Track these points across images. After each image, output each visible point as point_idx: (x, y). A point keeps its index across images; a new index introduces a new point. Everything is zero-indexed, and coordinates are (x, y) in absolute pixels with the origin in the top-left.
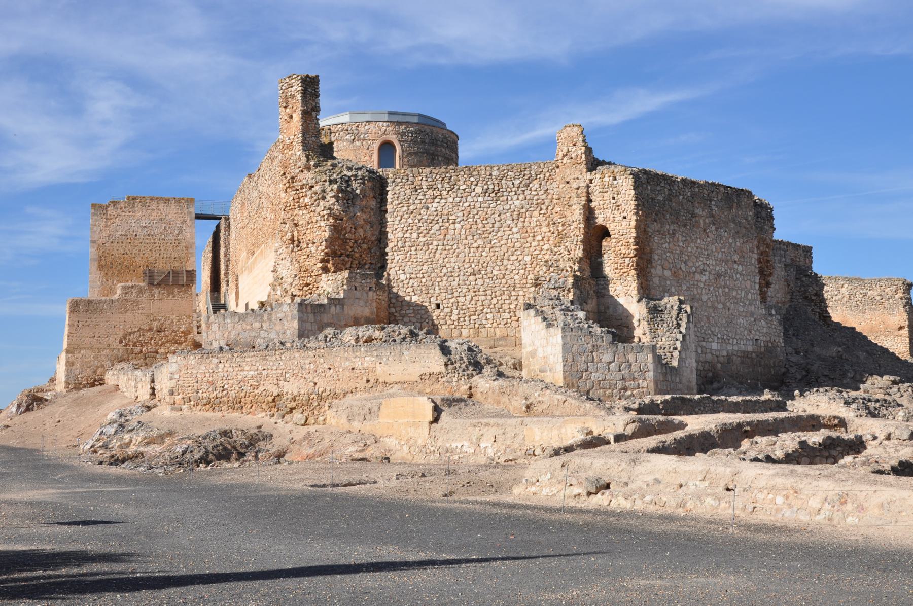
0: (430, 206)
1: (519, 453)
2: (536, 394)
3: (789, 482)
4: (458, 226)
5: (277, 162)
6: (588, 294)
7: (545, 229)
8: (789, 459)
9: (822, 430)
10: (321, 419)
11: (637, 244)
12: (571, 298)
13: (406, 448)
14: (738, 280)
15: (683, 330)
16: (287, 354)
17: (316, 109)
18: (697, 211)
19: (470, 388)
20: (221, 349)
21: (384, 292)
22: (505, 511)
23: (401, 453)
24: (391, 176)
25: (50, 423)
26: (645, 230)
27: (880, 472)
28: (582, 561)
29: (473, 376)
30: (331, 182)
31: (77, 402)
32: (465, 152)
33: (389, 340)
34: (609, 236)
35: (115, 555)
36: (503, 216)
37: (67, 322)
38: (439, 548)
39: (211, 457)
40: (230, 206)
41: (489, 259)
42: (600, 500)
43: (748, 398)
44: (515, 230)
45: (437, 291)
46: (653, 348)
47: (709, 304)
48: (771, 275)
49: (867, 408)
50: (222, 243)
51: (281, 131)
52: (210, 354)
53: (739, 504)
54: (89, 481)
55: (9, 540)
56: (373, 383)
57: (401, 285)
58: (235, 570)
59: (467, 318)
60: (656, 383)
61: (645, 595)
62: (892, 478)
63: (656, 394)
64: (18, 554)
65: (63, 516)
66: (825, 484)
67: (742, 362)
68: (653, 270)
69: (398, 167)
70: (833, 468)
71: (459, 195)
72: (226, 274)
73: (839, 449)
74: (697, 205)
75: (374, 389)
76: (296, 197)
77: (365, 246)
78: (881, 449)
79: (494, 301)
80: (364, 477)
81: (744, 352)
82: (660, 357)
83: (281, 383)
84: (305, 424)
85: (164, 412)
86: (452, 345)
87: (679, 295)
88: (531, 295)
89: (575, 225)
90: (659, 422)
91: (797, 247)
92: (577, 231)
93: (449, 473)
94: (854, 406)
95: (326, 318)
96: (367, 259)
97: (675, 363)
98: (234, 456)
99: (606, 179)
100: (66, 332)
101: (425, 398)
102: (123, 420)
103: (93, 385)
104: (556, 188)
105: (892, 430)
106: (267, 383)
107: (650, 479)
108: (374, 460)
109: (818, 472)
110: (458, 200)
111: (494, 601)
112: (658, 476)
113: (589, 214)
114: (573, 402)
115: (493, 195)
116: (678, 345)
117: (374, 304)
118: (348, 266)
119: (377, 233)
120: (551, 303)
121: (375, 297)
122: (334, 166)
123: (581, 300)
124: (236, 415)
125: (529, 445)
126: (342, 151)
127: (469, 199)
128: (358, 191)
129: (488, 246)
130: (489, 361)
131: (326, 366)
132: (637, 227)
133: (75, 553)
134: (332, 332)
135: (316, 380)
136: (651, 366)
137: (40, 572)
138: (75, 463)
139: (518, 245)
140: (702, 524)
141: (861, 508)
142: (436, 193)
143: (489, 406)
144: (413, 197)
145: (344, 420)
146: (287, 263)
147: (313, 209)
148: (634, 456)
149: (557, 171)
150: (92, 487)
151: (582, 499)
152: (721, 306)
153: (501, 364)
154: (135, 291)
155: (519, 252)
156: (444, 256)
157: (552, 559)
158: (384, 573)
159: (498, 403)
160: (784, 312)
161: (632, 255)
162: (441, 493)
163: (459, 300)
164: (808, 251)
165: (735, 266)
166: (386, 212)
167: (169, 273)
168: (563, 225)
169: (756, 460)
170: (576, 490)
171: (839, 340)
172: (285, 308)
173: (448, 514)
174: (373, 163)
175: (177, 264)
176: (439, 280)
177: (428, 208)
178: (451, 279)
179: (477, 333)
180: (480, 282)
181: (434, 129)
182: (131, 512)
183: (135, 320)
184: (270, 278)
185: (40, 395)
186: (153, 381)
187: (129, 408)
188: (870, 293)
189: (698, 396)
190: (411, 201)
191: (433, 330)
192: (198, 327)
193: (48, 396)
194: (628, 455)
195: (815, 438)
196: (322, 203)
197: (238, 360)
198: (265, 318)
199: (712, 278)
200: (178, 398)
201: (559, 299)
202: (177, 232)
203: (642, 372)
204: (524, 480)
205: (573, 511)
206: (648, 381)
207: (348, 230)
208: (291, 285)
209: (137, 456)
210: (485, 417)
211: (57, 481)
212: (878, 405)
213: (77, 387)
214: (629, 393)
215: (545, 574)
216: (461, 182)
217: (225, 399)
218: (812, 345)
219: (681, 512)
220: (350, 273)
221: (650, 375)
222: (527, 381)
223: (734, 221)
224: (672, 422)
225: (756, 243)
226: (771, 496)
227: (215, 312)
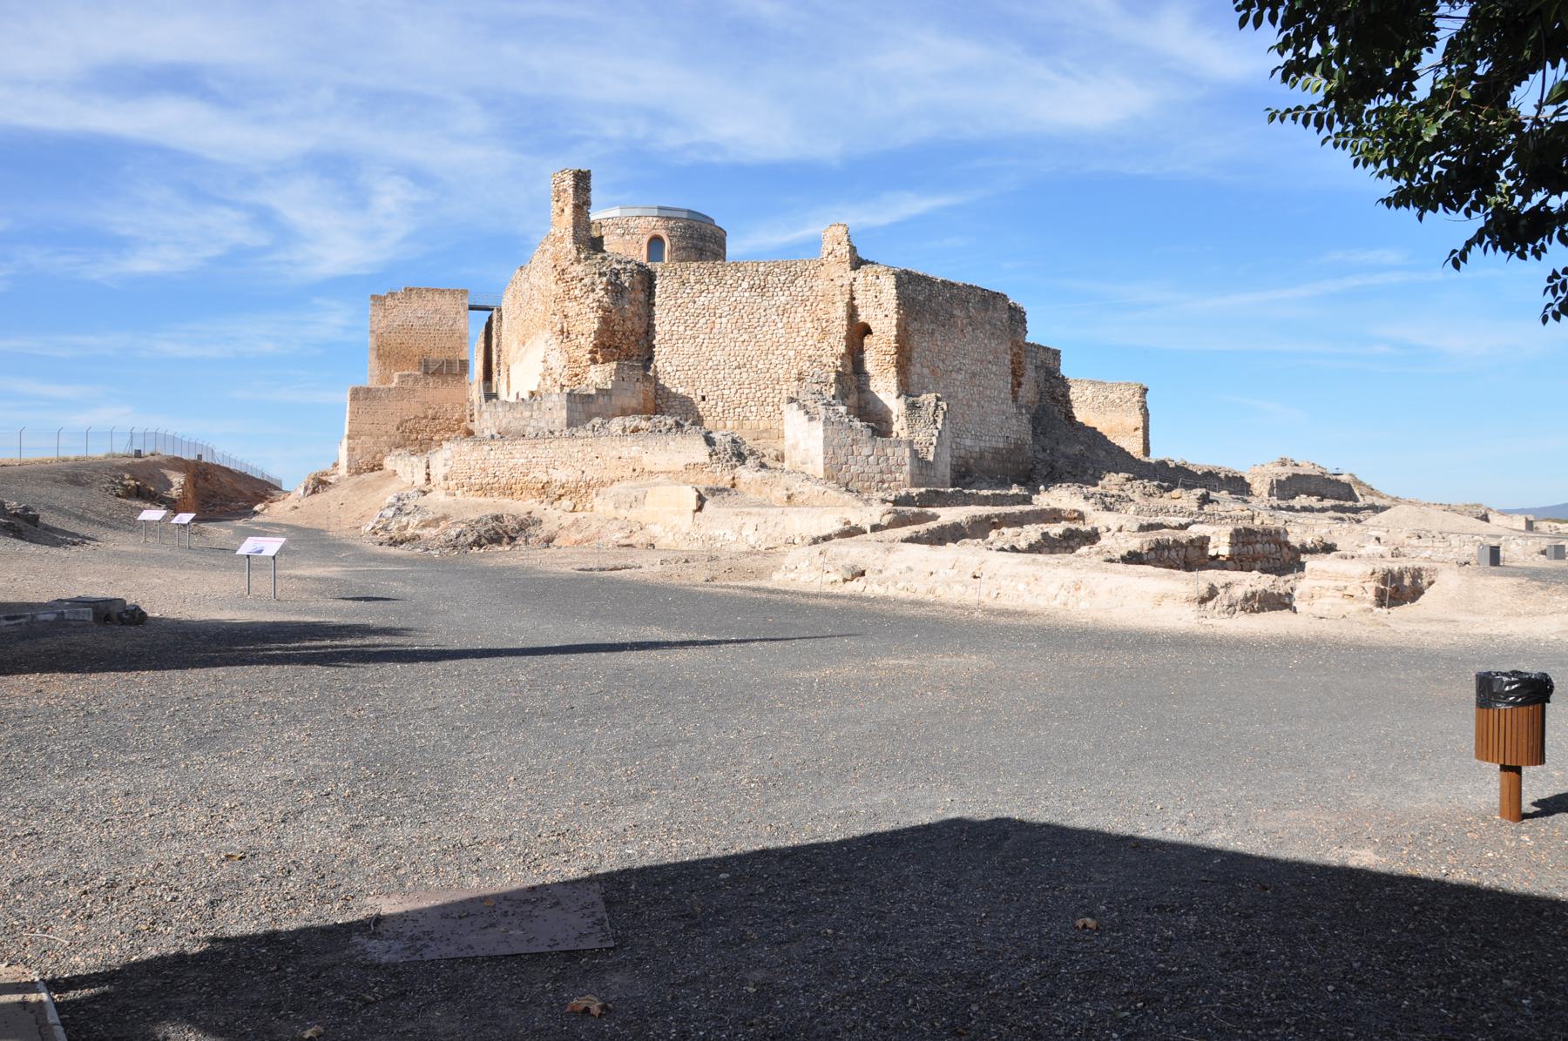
0: (697, 299)
1: (779, 542)
2: (797, 486)
3: (1031, 569)
4: (724, 320)
5: (548, 254)
6: (850, 389)
7: (809, 325)
8: (1032, 549)
9: (1063, 522)
10: (588, 506)
11: (897, 342)
12: (833, 393)
13: (670, 535)
14: (991, 379)
15: (939, 426)
16: (556, 443)
17: (587, 203)
18: (955, 312)
19: (733, 479)
20: (493, 437)
21: (651, 383)
22: (764, 596)
23: (665, 540)
24: (659, 269)
25: (334, 506)
26: (905, 329)
27: (1111, 561)
28: (836, 643)
29: (736, 466)
30: (601, 275)
31: (358, 486)
32: (733, 248)
33: (655, 431)
34: (871, 333)
35: (394, 629)
36: (768, 311)
37: (348, 409)
38: (701, 630)
39: (483, 541)
40: (501, 298)
41: (754, 353)
42: (856, 587)
43: (998, 492)
44: (780, 325)
45: (703, 384)
46: (911, 443)
47: (965, 402)
48: (1022, 375)
49: (1104, 503)
50: (494, 333)
51: (552, 224)
52: (482, 441)
53: (984, 591)
54: (370, 560)
55: (299, 612)
56: (638, 472)
57: (667, 377)
58: (506, 647)
59: (731, 411)
60: (912, 476)
61: (893, 673)
62: (1121, 566)
63: (911, 487)
64: (307, 625)
65: (347, 592)
66: (1062, 571)
67: (993, 458)
68: (912, 368)
69: (666, 261)
70: (1070, 557)
71: (726, 290)
72: (498, 364)
73: (1077, 540)
74: (956, 306)
75: (640, 478)
76: (566, 289)
77: (633, 338)
78: (1113, 540)
79: (759, 394)
80: (629, 562)
81: (995, 448)
82: (916, 451)
83: (550, 471)
84: (573, 511)
85: (439, 498)
86: (716, 436)
87: (936, 392)
88: (795, 389)
89: (838, 322)
90: (914, 514)
91: (1047, 349)
92: (840, 328)
93: (711, 559)
94: (1092, 501)
95: (594, 408)
96: (635, 351)
97: (931, 458)
98: (506, 540)
99: (869, 278)
100: (347, 419)
101: (690, 487)
102: (400, 503)
103: (372, 470)
104: (820, 285)
105: (1123, 522)
106: (537, 470)
107: (903, 567)
108: (639, 546)
109: (1057, 561)
110: (724, 294)
111: (751, 678)
112: (910, 564)
113: (852, 311)
114: (833, 493)
115: (759, 290)
116: (934, 440)
117: (642, 395)
118: (616, 357)
119: (645, 325)
120: (813, 397)
121: (642, 388)
122: (604, 259)
123: (842, 395)
124: (506, 500)
125: (788, 534)
126: (612, 244)
127: (736, 294)
128: (627, 284)
129: (754, 340)
130: (752, 453)
131: (594, 455)
132: (898, 326)
133: (359, 626)
134: (599, 422)
135: (583, 469)
136: (907, 460)
137: (328, 642)
138: (358, 543)
139: (782, 340)
140: (950, 609)
141: (1093, 594)
142: (704, 287)
143: (751, 495)
144: (681, 291)
145: (611, 507)
146: (556, 354)
147: (582, 301)
148: (889, 545)
149: (822, 268)
150: (373, 566)
151: (838, 585)
152: (975, 404)
153: (764, 456)
154: (410, 379)
155: (783, 347)
156: (709, 349)
157: (808, 640)
158: (647, 652)
159: (760, 493)
160: (1034, 411)
161: (892, 352)
162: (704, 578)
163: (725, 392)
164: (1056, 354)
165: (990, 366)
166: (654, 305)
167: (442, 365)
168: (827, 321)
169: (1002, 549)
170: (833, 577)
171: (1081, 439)
172: (555, 398)
173: (710, 598)
174: (642, 256)
175: (451, 354)
176: (705, 372)
177: (695, 302)
178: (717, 372)
179: (741, 425)
180: (745, 375)
181: (703, 225)
182: (409, 590)
183: (411, 408)
184: (540, 368)
185: (324, 478)
186: (428, 467)
187: (405, 493)
188: (1111, 396)
189: (951, 490)
190: (679, 295)
191: (698, 421)
192: (471, 416)
193: (332, 479)
194: (883, 545)
195: (1056, 530)
196: (591, 295)
197: (509, 447)
198: (535, 407)
199: (967, 376)
200: (452, 483)
201: (821, 393)
202: (451, 323)
203: (900, 465)
204: (783, 567)
205: (829, 596)
206: (904, 475)
207: (617, 321)
208: (561, 375)
209: (415, 538)
210: (747, 506)
211: (341, 560)
212: (1113, 500)
213: (358, 472)
214: (886, 485)
215: (800, 655)
216: (728, 277)
217: (497, 485)
218: (1058, 443)
219: (931, 598)
220: (618, 364)
221: (907, 468)
222: (788, 473)
223: (990, 323)
224: (925, 513)
225: (1009, 344)
226: (1013, 583)
227: (487, 401)
